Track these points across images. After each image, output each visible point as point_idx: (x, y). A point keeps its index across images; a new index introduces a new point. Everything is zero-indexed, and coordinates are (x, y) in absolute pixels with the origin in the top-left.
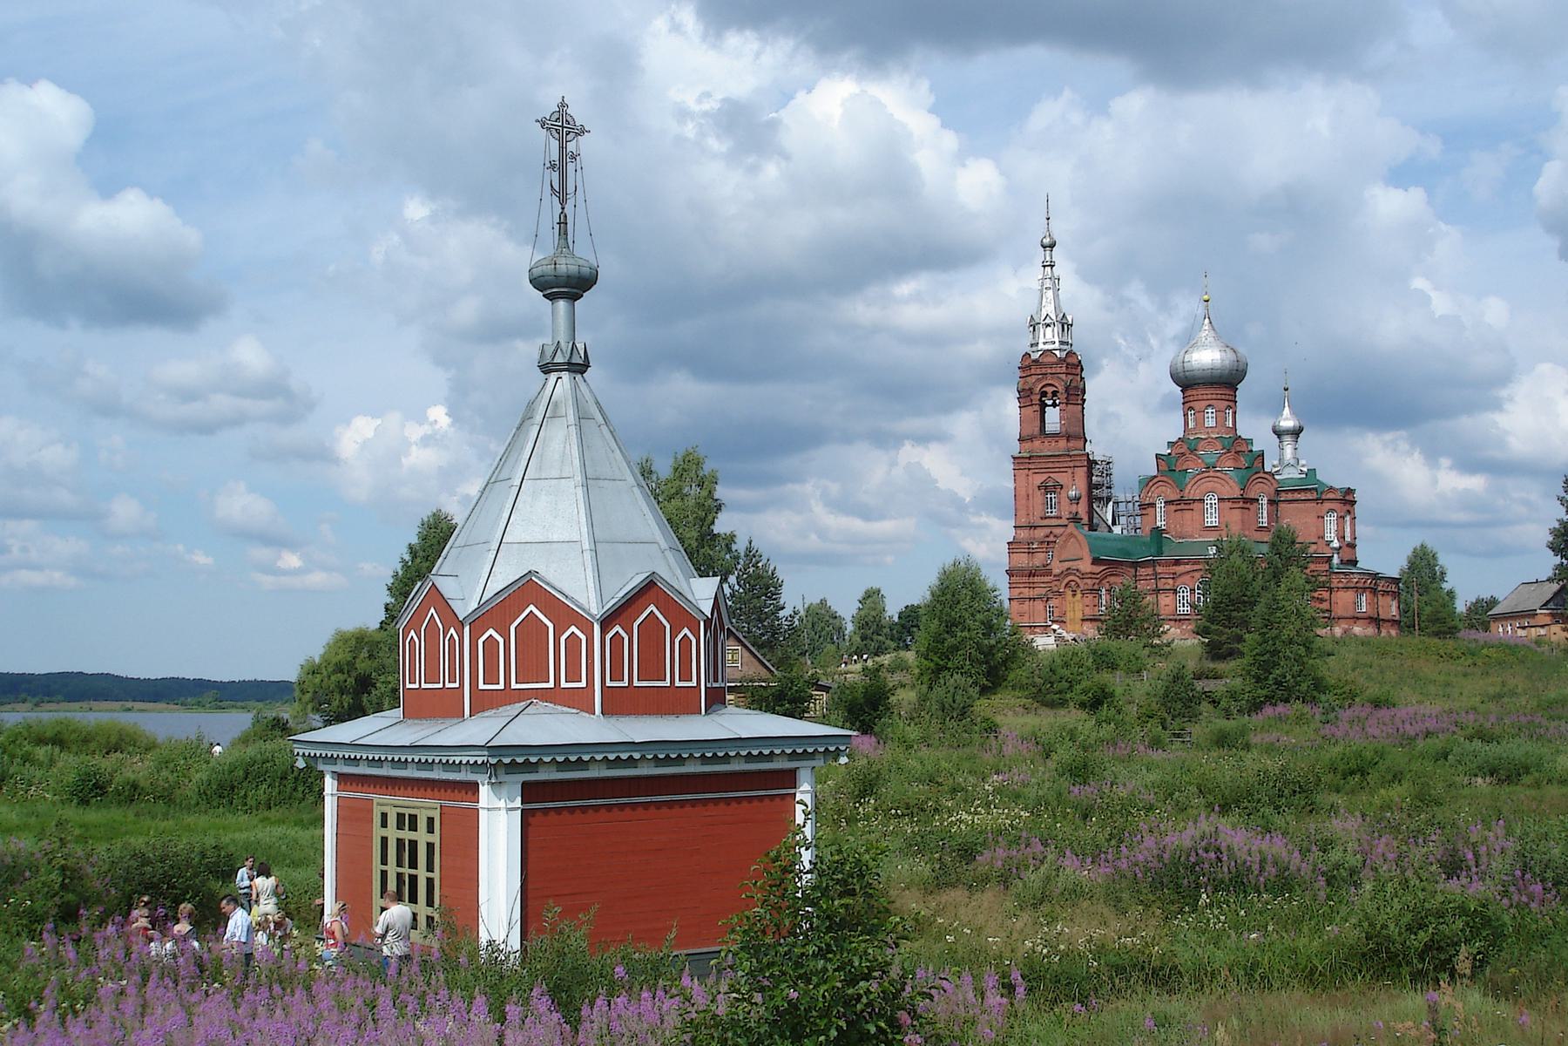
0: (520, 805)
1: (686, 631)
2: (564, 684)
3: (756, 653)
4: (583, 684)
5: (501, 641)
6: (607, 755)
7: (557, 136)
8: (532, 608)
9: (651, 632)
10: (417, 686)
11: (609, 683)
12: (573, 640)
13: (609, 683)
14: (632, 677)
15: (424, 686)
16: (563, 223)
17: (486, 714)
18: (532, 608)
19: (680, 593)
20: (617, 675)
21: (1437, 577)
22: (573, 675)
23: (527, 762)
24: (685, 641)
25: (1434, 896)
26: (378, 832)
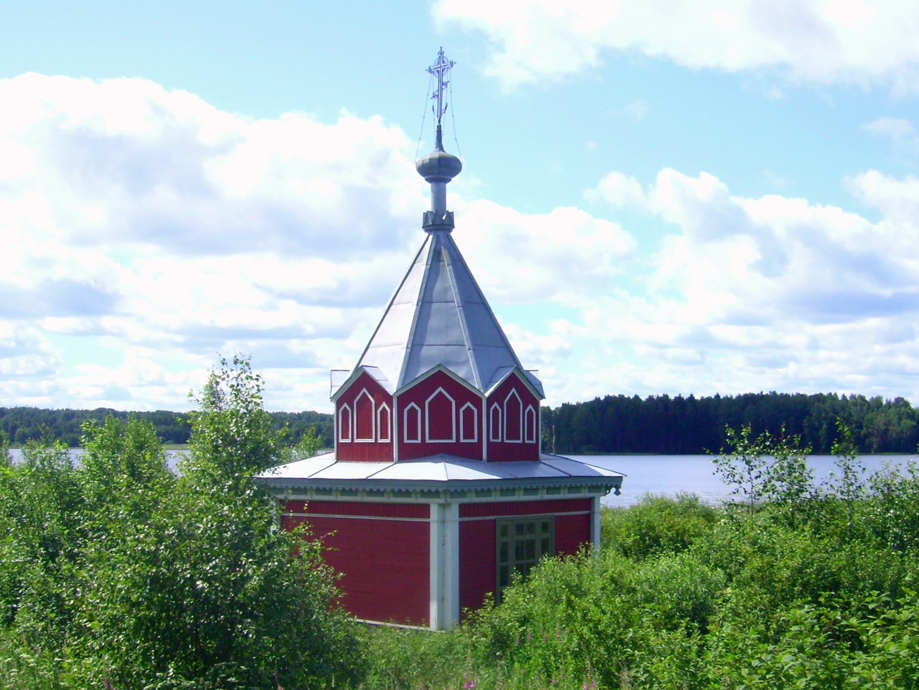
2: (462, 440)
3: (540, 425)
4: (475, 440)
5: (389, 410)
8: (440, 389)
10: (349, 441)
11: (406, 441)
12: (384, 409)
14: (502, 438)
15: (356, 441)
18: (440, 389)
20: (496, 435)
21: (694, 397)
22: (469, 434)
26: (500, 540)
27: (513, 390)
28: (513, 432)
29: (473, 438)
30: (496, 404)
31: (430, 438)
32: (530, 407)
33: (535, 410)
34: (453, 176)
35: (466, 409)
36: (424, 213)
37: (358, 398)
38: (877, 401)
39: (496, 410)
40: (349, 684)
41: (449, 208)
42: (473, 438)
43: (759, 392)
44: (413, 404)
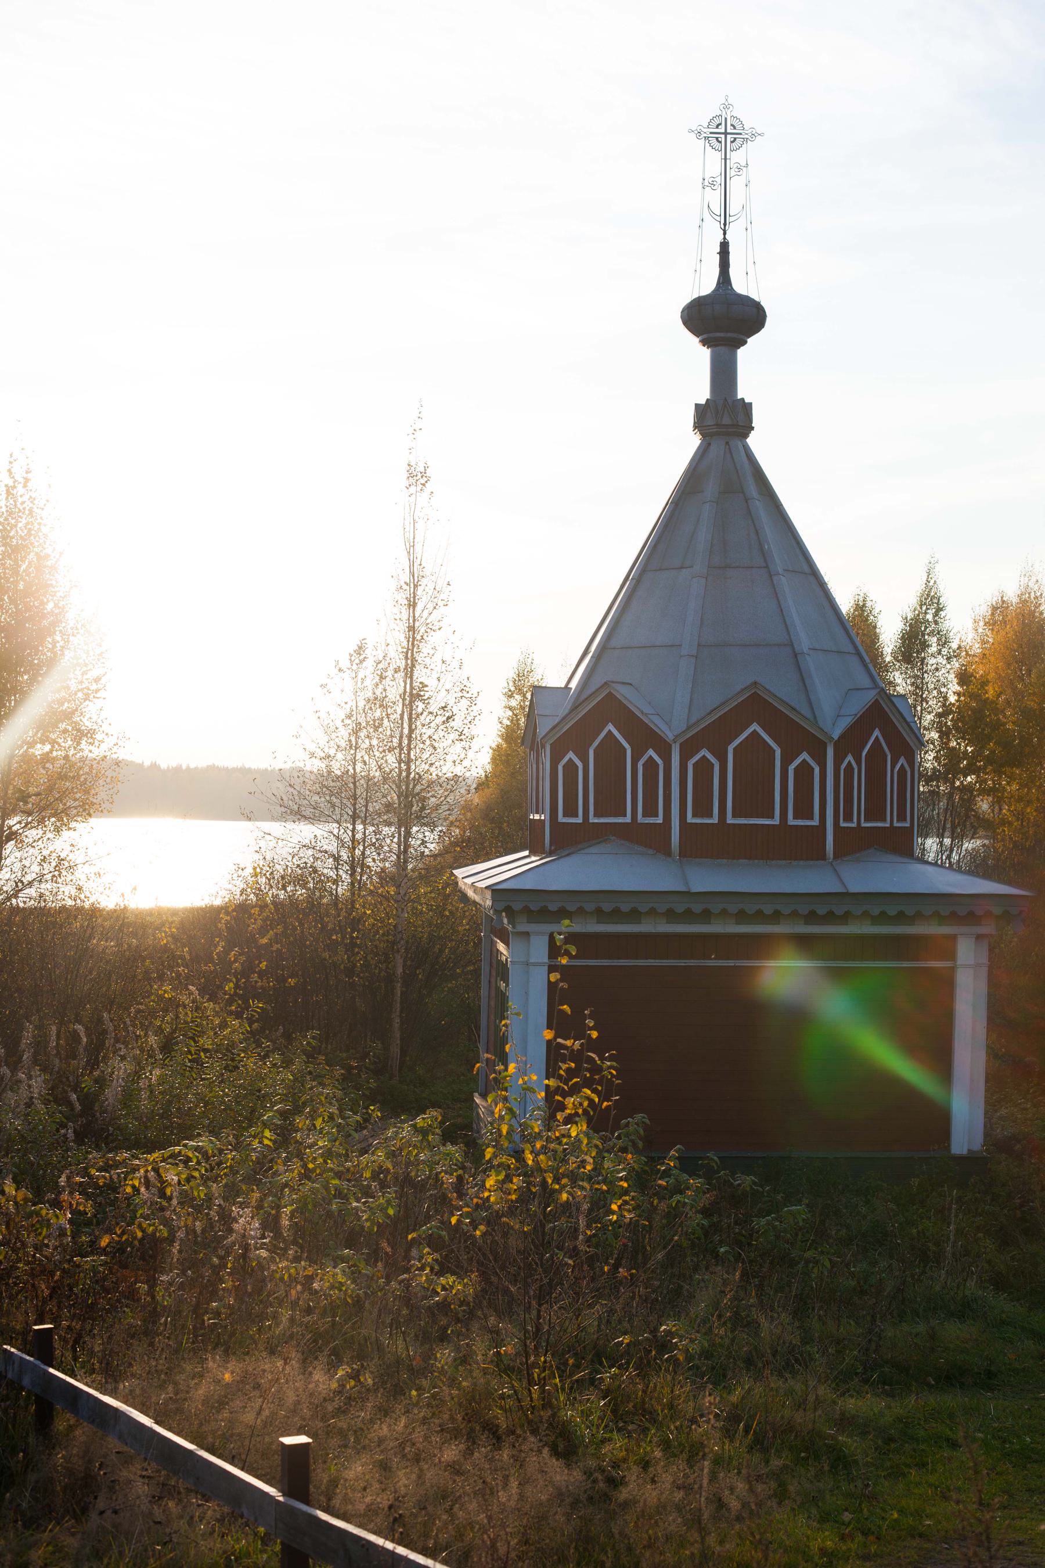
0: (546, 960)
1: (571, 755)
4: (815, 822)
6: (511, 904)
7: (717, 145)
8: (755, 727)
9: (610, 756)
11: (690, 819)
12: (651, 764)
13: (690, 819)
14: (859, 820)
16: (724, 250)
17: (593, 850)
18: (755, 727)
19: (794, 709)
20: (703, 807)
22: (650, 810)
23: (831, 913)
24: (804, 772)
25: (397, 1499)
27: (876, 733)
28: (875, 811)
29: (711, 816)
30: (850, 758)
31: (694, 815)
32: (902, 760)
33: (910, 766)
34: (749, 337)
35: (647, 761)
36: (697, 405)
37: (864, 754)
38: (250, 769)
39: (571, 767)
40: (66, 1229)
41: (743, 392)
42: (711, 816)
43: (491, 751)
44: (704, 752)
